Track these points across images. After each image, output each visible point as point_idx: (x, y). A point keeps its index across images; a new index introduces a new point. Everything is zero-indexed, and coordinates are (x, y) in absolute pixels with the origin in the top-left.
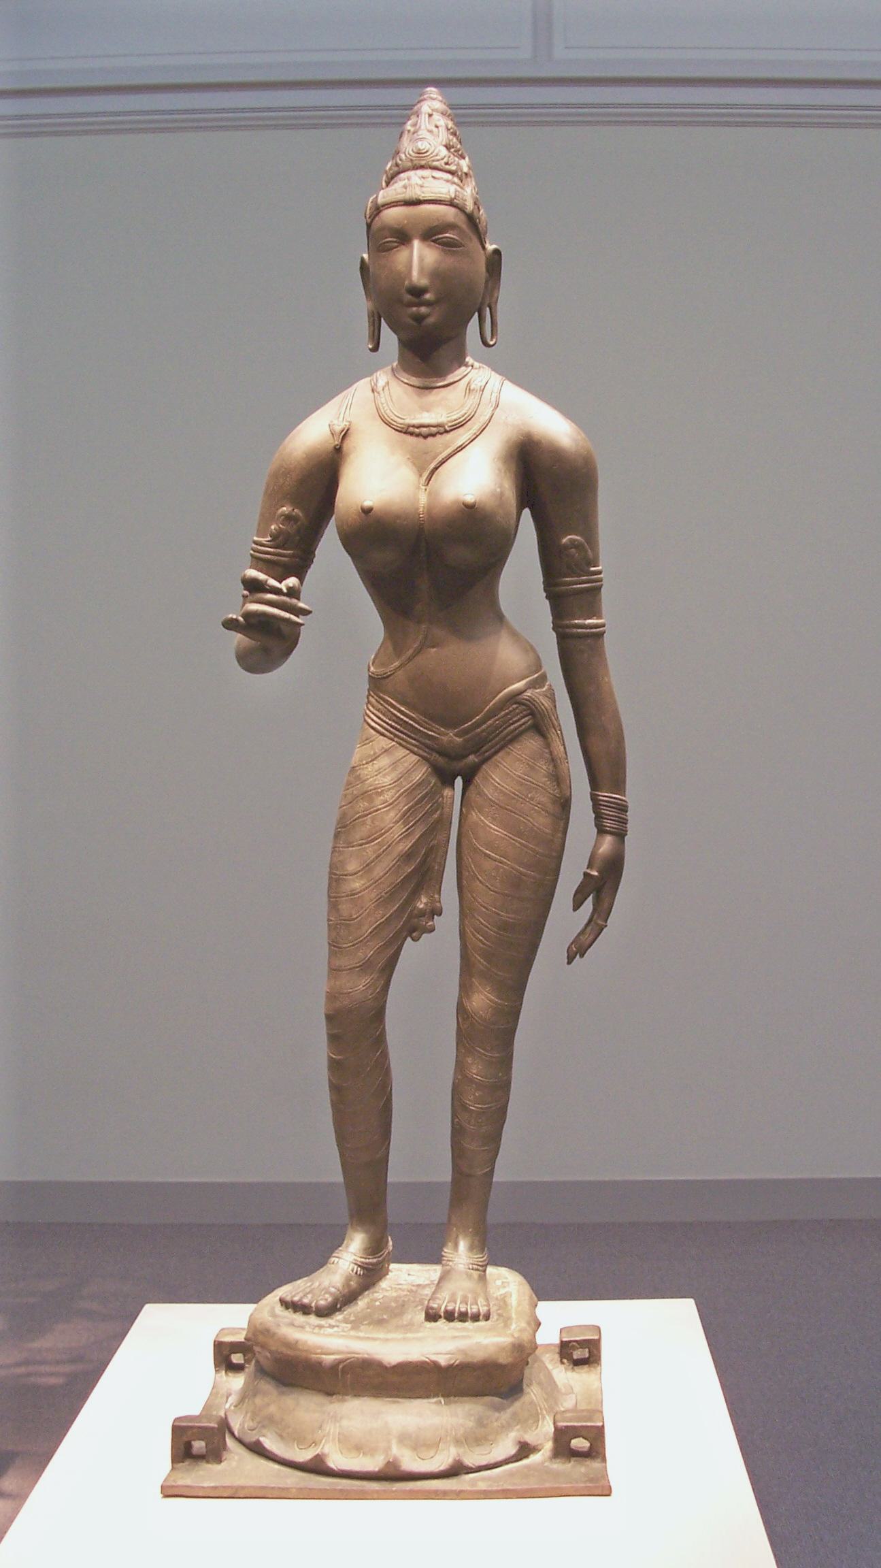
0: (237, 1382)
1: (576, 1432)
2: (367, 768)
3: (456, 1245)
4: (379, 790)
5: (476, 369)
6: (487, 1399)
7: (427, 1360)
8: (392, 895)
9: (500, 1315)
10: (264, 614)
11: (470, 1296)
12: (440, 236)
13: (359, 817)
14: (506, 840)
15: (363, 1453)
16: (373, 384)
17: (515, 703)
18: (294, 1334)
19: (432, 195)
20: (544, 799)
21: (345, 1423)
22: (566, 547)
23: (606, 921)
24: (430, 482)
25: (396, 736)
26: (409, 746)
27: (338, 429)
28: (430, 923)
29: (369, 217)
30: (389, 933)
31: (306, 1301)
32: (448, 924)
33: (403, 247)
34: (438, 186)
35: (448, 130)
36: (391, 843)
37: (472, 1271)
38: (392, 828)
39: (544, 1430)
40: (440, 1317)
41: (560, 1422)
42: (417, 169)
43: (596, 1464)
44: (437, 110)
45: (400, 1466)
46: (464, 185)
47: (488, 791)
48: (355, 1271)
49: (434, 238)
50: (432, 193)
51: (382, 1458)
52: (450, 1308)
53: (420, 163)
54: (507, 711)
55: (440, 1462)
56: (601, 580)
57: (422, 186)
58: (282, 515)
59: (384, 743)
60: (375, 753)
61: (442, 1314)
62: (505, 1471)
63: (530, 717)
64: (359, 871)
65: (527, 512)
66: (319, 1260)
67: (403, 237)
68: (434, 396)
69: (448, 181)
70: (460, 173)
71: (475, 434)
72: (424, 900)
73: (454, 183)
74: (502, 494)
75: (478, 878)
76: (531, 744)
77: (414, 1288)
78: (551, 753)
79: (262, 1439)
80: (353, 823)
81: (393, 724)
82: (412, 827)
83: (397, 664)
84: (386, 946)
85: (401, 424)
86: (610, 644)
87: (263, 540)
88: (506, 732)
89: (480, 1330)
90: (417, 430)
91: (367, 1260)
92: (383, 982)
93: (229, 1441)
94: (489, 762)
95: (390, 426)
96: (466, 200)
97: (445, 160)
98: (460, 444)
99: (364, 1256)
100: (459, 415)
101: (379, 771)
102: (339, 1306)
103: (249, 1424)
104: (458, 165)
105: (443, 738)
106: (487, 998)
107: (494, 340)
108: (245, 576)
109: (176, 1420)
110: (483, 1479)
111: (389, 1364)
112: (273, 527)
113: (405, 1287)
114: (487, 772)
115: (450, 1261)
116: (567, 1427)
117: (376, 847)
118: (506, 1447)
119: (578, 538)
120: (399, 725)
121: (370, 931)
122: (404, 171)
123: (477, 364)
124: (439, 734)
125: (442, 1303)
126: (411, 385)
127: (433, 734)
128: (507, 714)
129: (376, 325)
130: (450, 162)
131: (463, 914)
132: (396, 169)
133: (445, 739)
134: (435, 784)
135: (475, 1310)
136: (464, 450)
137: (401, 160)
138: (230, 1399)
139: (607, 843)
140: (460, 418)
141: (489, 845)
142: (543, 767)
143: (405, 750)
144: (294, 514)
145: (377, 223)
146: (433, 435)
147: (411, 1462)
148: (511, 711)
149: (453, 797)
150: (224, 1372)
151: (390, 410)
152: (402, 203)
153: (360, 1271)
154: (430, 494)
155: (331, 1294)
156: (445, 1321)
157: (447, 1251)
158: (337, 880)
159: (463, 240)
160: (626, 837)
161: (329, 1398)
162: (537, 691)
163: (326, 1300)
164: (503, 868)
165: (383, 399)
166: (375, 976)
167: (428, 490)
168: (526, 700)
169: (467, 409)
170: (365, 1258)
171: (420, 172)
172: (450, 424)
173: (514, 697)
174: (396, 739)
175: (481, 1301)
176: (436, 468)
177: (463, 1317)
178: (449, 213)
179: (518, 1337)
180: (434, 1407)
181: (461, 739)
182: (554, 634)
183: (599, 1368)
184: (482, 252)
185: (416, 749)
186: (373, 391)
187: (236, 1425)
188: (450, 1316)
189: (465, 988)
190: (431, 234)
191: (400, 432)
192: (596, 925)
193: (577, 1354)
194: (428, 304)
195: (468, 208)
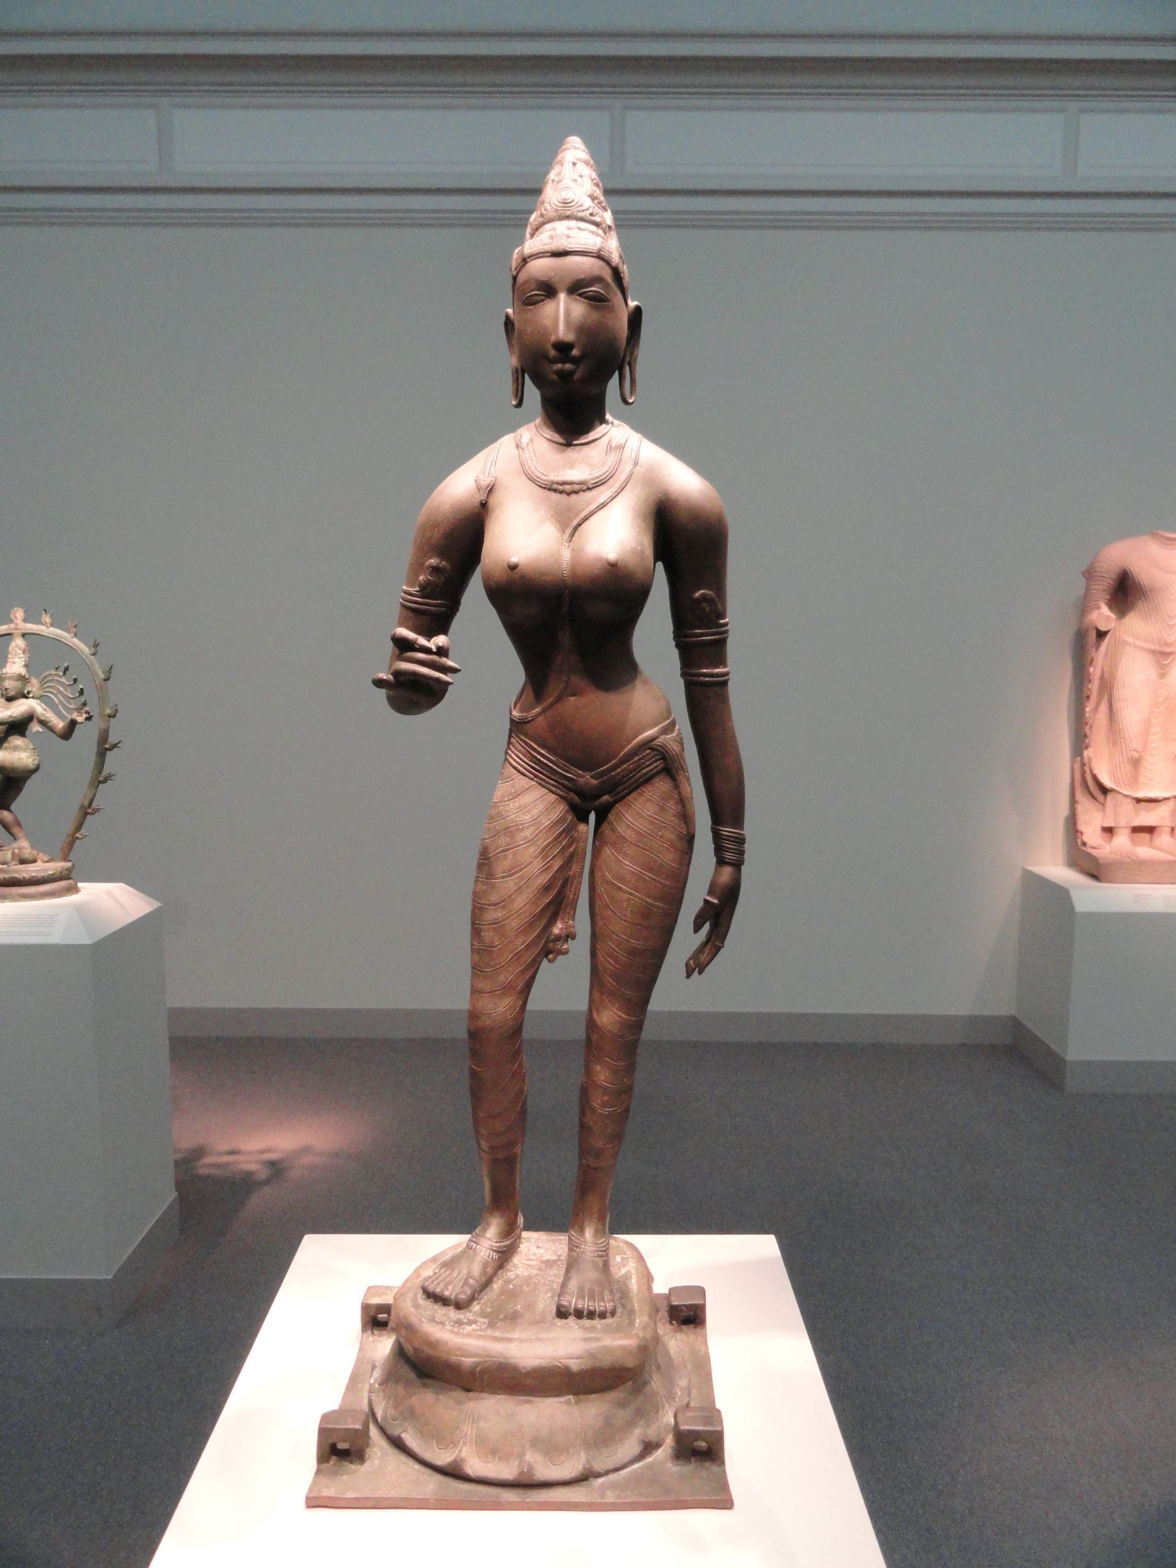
2: (508, 804)
5: (616, 426)
8: (531, 924)
10: (415, 674)
12: (586, 290)
15: (499, 1458)
16: (517, 440)
17: (649, 749)
19: (581, 246)
20: (672, 837)
21: (482, 1424)
22: (698, 601)
23: (723, 944)
24: (573, 539)
25: (536, 776)
26: (547, 785)
29: (516, 269)
30: (528, 958)
31: (447, 1293)
33: (549, 300)
34: (583, 237)
35: (592, 180)
36: (531, 877)
37: (598, 1259)
39: (665, 1421)
40: (570, 1314)
41: (683, 1425)
42: (562, 219)
44: (580, 160)
45: (534, 1475)
46: (608, 238)
48: (490, 1257)
50: (579, 244)
53: (566, 214)
54: (641, 756)
56: (726, 632)
59: (524, 782)
60: (516, 792)
62: (631, 1473)
63: (661, 761)
65: (660, 565)
67: (548, 290)
68: (572, 454)
69: (593, 233)
70: (604, 226)
71: (616, 491)
73: (598, 235)
74: (642, 552)
76: (662, 785)
78: (680, 794)
79: (403, 1435)
80: (496, 856)
81: (534, 765)
82: (549, 862)
83: (538, 710)
84: (523, 972)
85: (545, 481)
86: (733, 689)
87: (412, 590)
89: (608, 1330)
92: (521, 1002)
94: (622, 802)
95: (533, 482)
96: (611, 253)
97: (590, 211)
98: (602, 501)
100: (600, 473)
101: (520, 808)
104: (602, 217)
106: (616, 1014)
107: (633, 398)
108: (395, 634)
109: (325, 1417)
111: (524, 1369)
112: (421, 578)
115: (577, 1247)
119: (710, 592)
120: (539, 766)
121: (510, 956)
123: (616, 422)
125: (572, 1301)
126: (554, 442)
127: (571, 776)
128: (641, 759)
129: (520, 381)
130: (594, 214)
131: (594, 937)
132: (542, 219)
133: (582, 780)
134: (571, 821)
136: (605, 508)
139: (727, 873)
140: (601, 476)
142: (672, 807)
143: (544, 789)
144: (441, 565)
145: (522, 277)
146: (576, 492)
147: (546, 1471)
148: (644, 757)
149: (587, 833)
150: (370, 1331)
151: (535, 466)
152: (549, 254)
153: (495, 1256)
154: (573, 550)
156: (575, 1318)
158: (481, 909)
159: (608, 295)
162: (667, 737)
164: (633, 900)
165: (527, 455)
167: (571, 546)
168: (658, 745)
169: (609, 466)
171: (565, 223)
172: (592, 482)
173: (647, 744)
174: (535, 779)
176: (579, 525)
177: (591, 1315)
180: (565, 1407)
181: (598, 781)
182: (682, 681)
184: (626, 309)
185: (554, 789)
186: (518, 447)
188: (579, 1314)
190: (576, 288)
191: (545, 488)
194: (575, 361)
195: (614, 260)
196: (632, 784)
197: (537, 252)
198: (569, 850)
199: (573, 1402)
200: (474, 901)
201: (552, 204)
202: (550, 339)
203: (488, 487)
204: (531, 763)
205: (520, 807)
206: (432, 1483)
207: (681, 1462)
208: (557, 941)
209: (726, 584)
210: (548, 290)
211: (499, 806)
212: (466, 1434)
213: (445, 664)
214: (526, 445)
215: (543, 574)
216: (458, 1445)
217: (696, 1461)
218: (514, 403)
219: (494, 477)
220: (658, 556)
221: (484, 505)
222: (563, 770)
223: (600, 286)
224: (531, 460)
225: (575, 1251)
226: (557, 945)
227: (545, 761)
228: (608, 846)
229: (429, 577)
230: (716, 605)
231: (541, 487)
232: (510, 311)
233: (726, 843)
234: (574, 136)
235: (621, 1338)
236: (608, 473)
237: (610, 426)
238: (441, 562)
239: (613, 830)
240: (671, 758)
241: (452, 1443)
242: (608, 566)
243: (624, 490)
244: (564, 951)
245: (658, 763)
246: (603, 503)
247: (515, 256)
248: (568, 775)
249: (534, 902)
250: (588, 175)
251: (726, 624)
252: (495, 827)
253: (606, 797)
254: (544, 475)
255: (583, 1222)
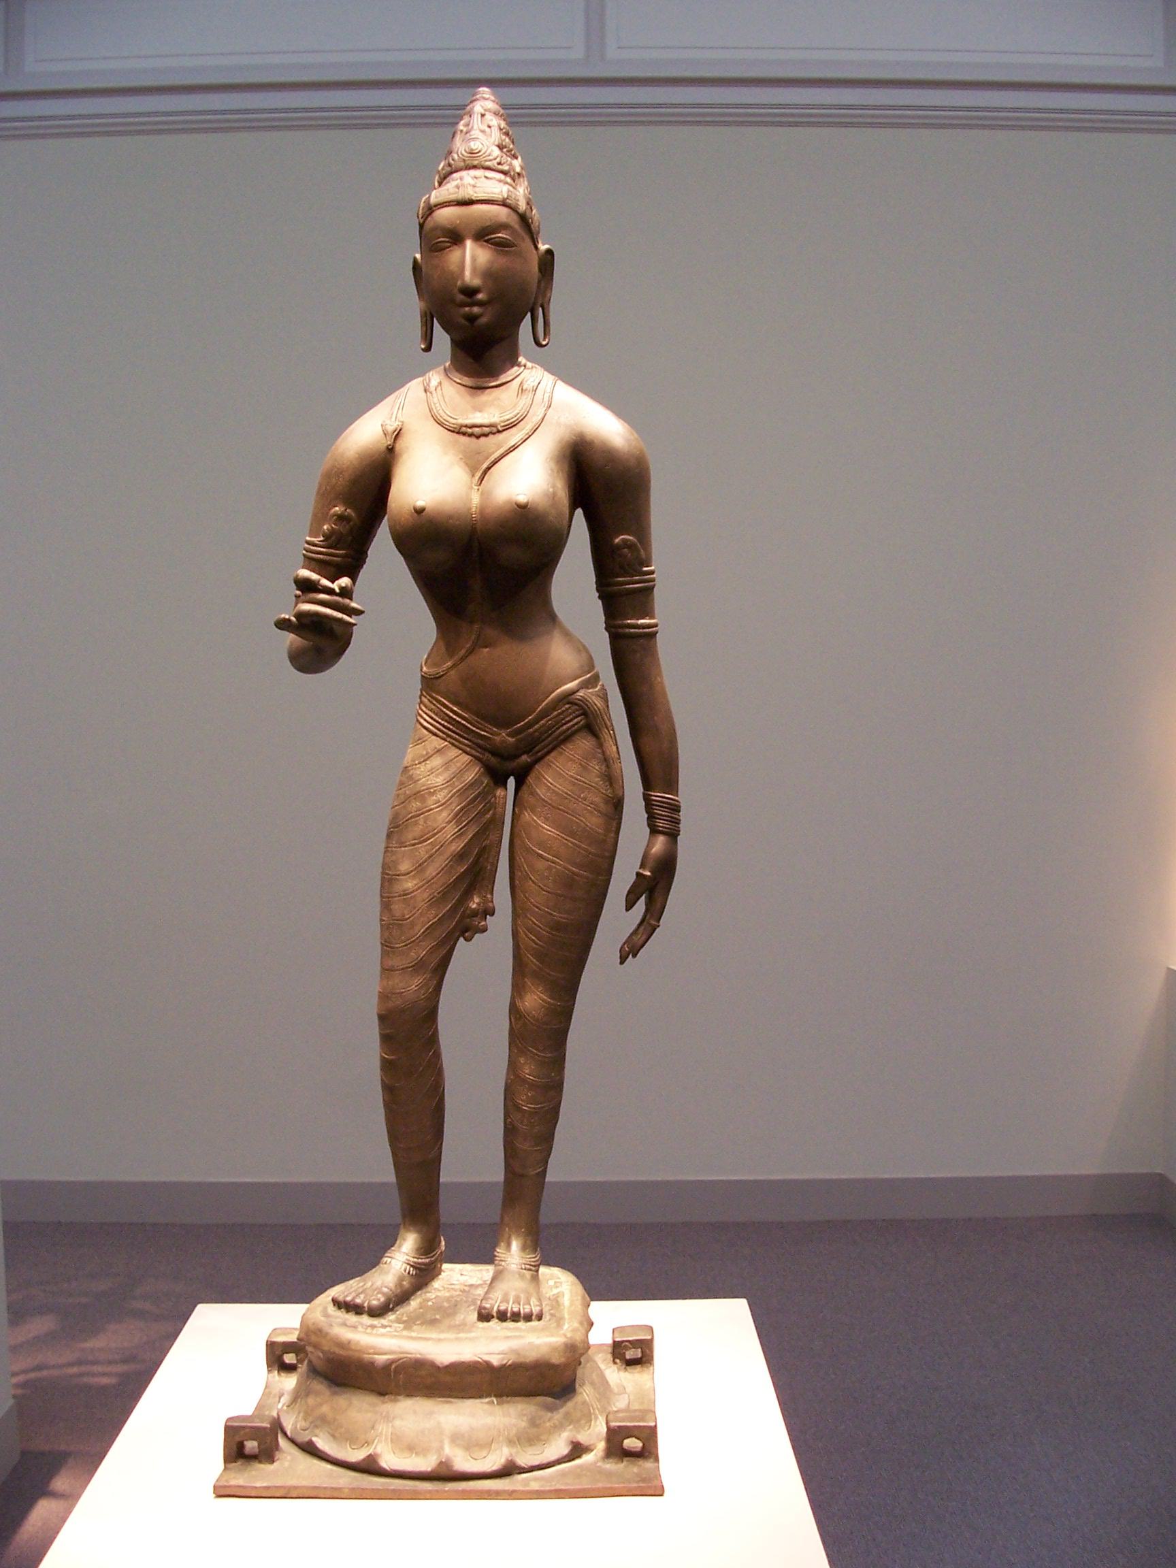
0: (289, 1382)
1: (628, 1432)
3: (509, 1245)
4: (432, 790)
5: (528, 369)
6: (540, 1399)
7: (480, 1360)
8: (445, 895)
9: (552, 1315)
10: (317, 614)
11: (522, 1296)
13: (411, 818)
14: (559, 839)
15: (416, 1453)
16: (425, 384)
17: (568, 703)
18: (346, 1335)
21: (397, 1423)
22: (618, 547)
24: (483, 482)
27: (390, 429)
28: (483, 923)
29: (422, 218)
30: (441, 933)
31: (358, 1301)
32: (500, 925)
33: (455, 247)
35: (501, 129)
37: (524, 1271)
38: (444, 828)
40: (493, 1317)
42: (470, 169)
43: (648, 1464)
44: (489, 111)
45: (452, 1466)
46: (516, 185)
47: (541, 792)
48: (407, 1271)
49: (486, 238)
50: (485, 193)
51: (435, 1457)
52: (503, 1308)
53: (472, 164)
55: (493, 1462)
57: (474, 186)
58: (335, 514)
59: (436, 743)
60: (427, 753)
61: (495, 1314)
62: (557, 1471)
63: (583, 717)
64: (412, 871)
65: (579, 512)
66: (370, 1260)
67: (455, 237)
69: (500, 181)
70: (512, 174)
71: (528, 433)
72: (477, 900)
73: (506, 183)
74: (554, 494)
75: (530, 878)
76: (584, 743)
77: (466, 1288)
78: (604, 753)
79: (314, 1439)
81: (446, 724)
83: (449, 664)
85: (453, 424)
86: (662, 643)
88: (559, 731)
89: (533, 1330)
90: (469, 430)
91: (420, 1260)
93: (282, 1442)
94: (542, 763)
95: (442, 426)
96: (518, 200)
97: (498, 160)
98: (513, 444)
99: (416, 1256)
100: (511, 415)
101: (432, 771)
102: (391, 1306)
103: (301, 1424)
104: (510, 165)
105: (495, 738)
108: (297, 576)
109: (229, 1419)
110: (536, 1479)
111: (442, 1364)
112: (325, 527)
113: (457, 1287)
114: (539, 772)
115: (502, 1261)
116: (619, 1427)
117: (429, 847)
118: (558, 1447)
119: (631, 538)
122: (456, 171)
123: (529, 364)
124: (491, 734)
125: (495, 1303)
126: (463, 385)
128: (560, 714)
129: (429, 326)
130: (502, 162)
132: (449, 169)
135: (527, 1310)
137: (453, 160)
138: (282, 1399)
139: (660, 843)
141: (541, 845)
142: (596, 767)
143: (457, 750)
145: (430, 223)
146: (486, 435)
147: (464, 1464)
148: (563, 712)
149: (505, 797)
150: (276, 1372)
152: (455, 203)
153: (413, 1271)
154: (482, 494)
155: (384, 1294)
156: (497, 1321)
157: (500, 1251)
158: (390, 881)
160: (679, 837)
161: (382, 1398)
162: (590, 691)
163: (379, 1300)
164: (556, 868)
166: (427, 975)
167: (480, 490)
168: (579, 700)
169: (520, 408)
170: (418, 1258)
171: (473, 172)
172: (502, 424)
173: (567, 697)
174: (448, 739)
175: (534, 1301)
176: (489, 468)
177: (516, 1317)
178: (502, 213)
179: (571, 1338)
180: (486, 1407)
181: (514, 739)
183: (651, 1368)
185: (468, 749)
186: (425, 391)
187: (289, 1424)
188: (502, 1316)
189: (518, 988)
190: (484, 234)
191: (453, 432)
192: (649, 925)
193: (630, 1354)
194: (480, 304)
196: (552, 742)
197: (442, 201)
198: (486, 817)
199: (496, 1403)
200: (383, 873)
201: (459, 154)
202: (457, 283)
203: (395, 431)
204: (443, 722)
205: (432, 770)
206: (347, 1479)
207: (611, 1461)
208: (473, 917)
209: (650, 533)
210: (455, 237)
211: (409, 771)
212: (381, 1433)
213: (348, 605)
214: (434, 388)
215: (451, 517)
216: (373, 1443)
217: (628, 1461)
218: (423, 346)
219: (401, 422)
220: (574, 506)
221: (391, 450)
222: (471, 724)
223: (508, 232)
224: (440, 404)
225: (501, 1265)
226: (474, 921)
227: (458, 719)
228: (526, 810)
229: (333, 526)
230: (638, 551)
231: (449, 430)
232: (418, 256)
233: (656, 809)
234: (483, 87)
235: (547, 1336)
236: (519, 416)
237: (523, 368)
238: (346, 510)
239: (533, 793)
240: (593, 714)
241: (366, 1443)
242: (516, 506)
243: (536, 432)
244: (481, 928)
245: (579, 718)
246: (514, 445)
247: (422, 205)
248: (483, 733)
249: (448, 869)
250: (496, 125)
251: (652, 572)
252: (405, 793)
253: (525, 758)
254: (454, 419)
255: (510, 1237)
